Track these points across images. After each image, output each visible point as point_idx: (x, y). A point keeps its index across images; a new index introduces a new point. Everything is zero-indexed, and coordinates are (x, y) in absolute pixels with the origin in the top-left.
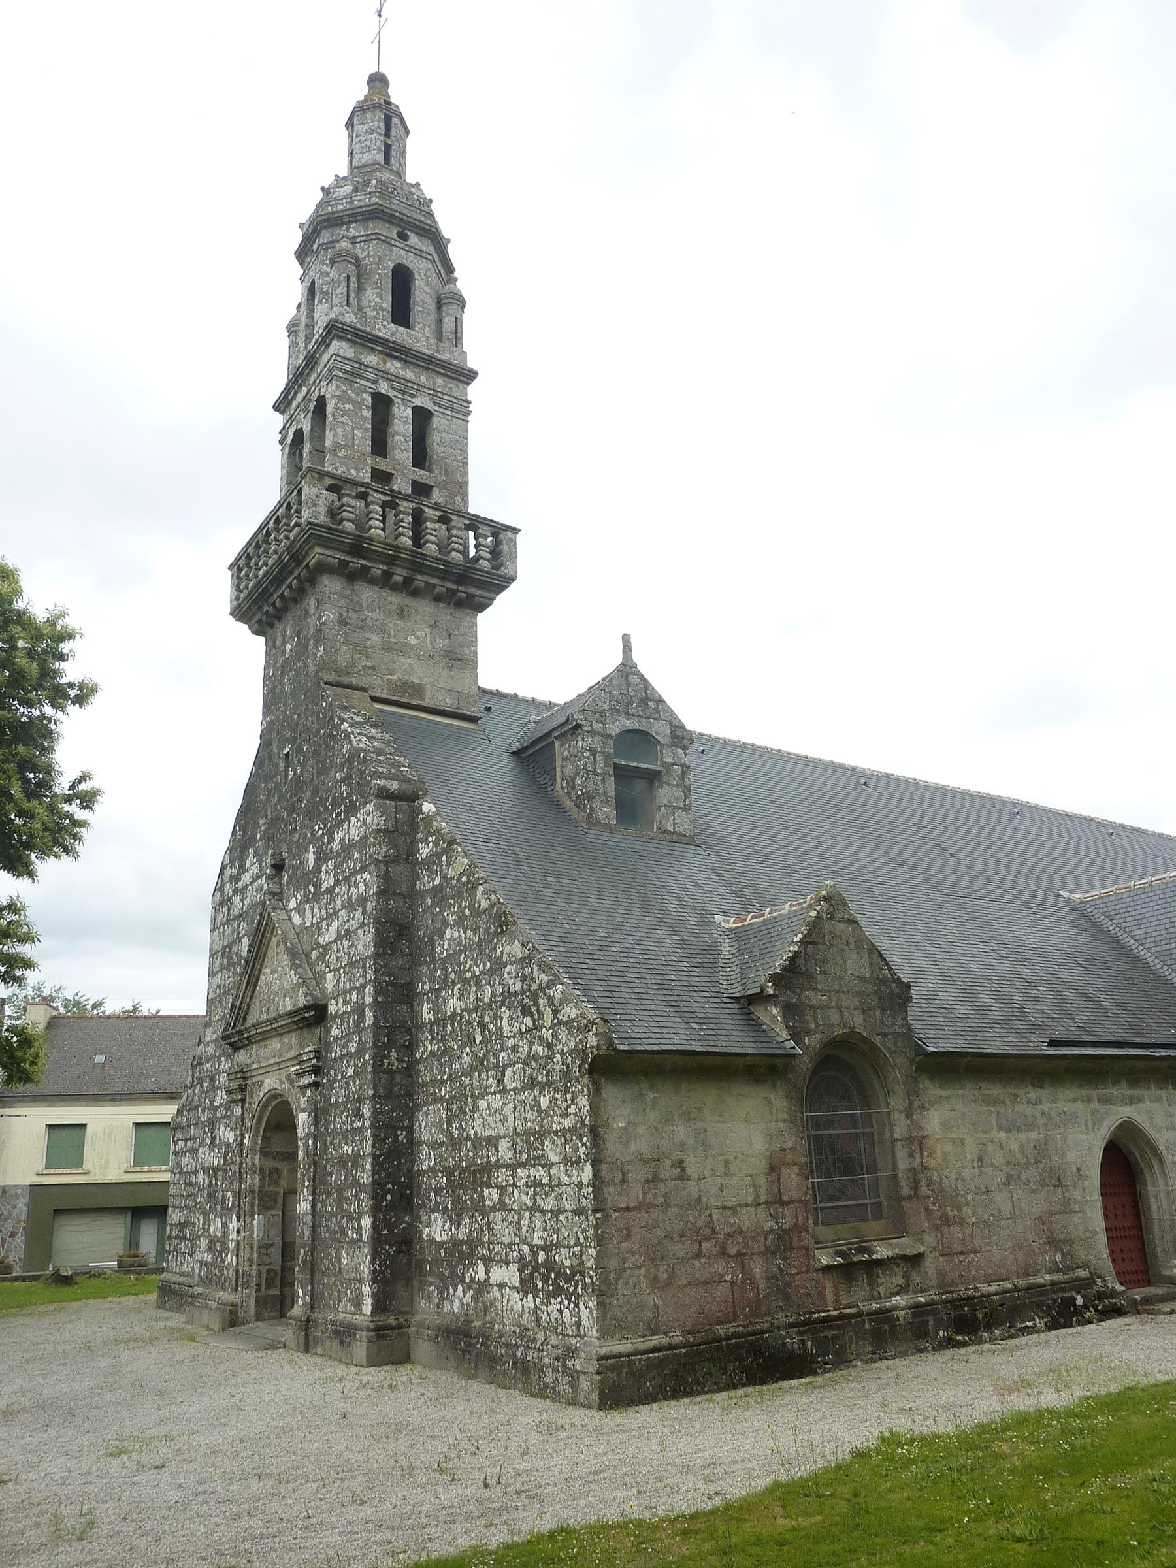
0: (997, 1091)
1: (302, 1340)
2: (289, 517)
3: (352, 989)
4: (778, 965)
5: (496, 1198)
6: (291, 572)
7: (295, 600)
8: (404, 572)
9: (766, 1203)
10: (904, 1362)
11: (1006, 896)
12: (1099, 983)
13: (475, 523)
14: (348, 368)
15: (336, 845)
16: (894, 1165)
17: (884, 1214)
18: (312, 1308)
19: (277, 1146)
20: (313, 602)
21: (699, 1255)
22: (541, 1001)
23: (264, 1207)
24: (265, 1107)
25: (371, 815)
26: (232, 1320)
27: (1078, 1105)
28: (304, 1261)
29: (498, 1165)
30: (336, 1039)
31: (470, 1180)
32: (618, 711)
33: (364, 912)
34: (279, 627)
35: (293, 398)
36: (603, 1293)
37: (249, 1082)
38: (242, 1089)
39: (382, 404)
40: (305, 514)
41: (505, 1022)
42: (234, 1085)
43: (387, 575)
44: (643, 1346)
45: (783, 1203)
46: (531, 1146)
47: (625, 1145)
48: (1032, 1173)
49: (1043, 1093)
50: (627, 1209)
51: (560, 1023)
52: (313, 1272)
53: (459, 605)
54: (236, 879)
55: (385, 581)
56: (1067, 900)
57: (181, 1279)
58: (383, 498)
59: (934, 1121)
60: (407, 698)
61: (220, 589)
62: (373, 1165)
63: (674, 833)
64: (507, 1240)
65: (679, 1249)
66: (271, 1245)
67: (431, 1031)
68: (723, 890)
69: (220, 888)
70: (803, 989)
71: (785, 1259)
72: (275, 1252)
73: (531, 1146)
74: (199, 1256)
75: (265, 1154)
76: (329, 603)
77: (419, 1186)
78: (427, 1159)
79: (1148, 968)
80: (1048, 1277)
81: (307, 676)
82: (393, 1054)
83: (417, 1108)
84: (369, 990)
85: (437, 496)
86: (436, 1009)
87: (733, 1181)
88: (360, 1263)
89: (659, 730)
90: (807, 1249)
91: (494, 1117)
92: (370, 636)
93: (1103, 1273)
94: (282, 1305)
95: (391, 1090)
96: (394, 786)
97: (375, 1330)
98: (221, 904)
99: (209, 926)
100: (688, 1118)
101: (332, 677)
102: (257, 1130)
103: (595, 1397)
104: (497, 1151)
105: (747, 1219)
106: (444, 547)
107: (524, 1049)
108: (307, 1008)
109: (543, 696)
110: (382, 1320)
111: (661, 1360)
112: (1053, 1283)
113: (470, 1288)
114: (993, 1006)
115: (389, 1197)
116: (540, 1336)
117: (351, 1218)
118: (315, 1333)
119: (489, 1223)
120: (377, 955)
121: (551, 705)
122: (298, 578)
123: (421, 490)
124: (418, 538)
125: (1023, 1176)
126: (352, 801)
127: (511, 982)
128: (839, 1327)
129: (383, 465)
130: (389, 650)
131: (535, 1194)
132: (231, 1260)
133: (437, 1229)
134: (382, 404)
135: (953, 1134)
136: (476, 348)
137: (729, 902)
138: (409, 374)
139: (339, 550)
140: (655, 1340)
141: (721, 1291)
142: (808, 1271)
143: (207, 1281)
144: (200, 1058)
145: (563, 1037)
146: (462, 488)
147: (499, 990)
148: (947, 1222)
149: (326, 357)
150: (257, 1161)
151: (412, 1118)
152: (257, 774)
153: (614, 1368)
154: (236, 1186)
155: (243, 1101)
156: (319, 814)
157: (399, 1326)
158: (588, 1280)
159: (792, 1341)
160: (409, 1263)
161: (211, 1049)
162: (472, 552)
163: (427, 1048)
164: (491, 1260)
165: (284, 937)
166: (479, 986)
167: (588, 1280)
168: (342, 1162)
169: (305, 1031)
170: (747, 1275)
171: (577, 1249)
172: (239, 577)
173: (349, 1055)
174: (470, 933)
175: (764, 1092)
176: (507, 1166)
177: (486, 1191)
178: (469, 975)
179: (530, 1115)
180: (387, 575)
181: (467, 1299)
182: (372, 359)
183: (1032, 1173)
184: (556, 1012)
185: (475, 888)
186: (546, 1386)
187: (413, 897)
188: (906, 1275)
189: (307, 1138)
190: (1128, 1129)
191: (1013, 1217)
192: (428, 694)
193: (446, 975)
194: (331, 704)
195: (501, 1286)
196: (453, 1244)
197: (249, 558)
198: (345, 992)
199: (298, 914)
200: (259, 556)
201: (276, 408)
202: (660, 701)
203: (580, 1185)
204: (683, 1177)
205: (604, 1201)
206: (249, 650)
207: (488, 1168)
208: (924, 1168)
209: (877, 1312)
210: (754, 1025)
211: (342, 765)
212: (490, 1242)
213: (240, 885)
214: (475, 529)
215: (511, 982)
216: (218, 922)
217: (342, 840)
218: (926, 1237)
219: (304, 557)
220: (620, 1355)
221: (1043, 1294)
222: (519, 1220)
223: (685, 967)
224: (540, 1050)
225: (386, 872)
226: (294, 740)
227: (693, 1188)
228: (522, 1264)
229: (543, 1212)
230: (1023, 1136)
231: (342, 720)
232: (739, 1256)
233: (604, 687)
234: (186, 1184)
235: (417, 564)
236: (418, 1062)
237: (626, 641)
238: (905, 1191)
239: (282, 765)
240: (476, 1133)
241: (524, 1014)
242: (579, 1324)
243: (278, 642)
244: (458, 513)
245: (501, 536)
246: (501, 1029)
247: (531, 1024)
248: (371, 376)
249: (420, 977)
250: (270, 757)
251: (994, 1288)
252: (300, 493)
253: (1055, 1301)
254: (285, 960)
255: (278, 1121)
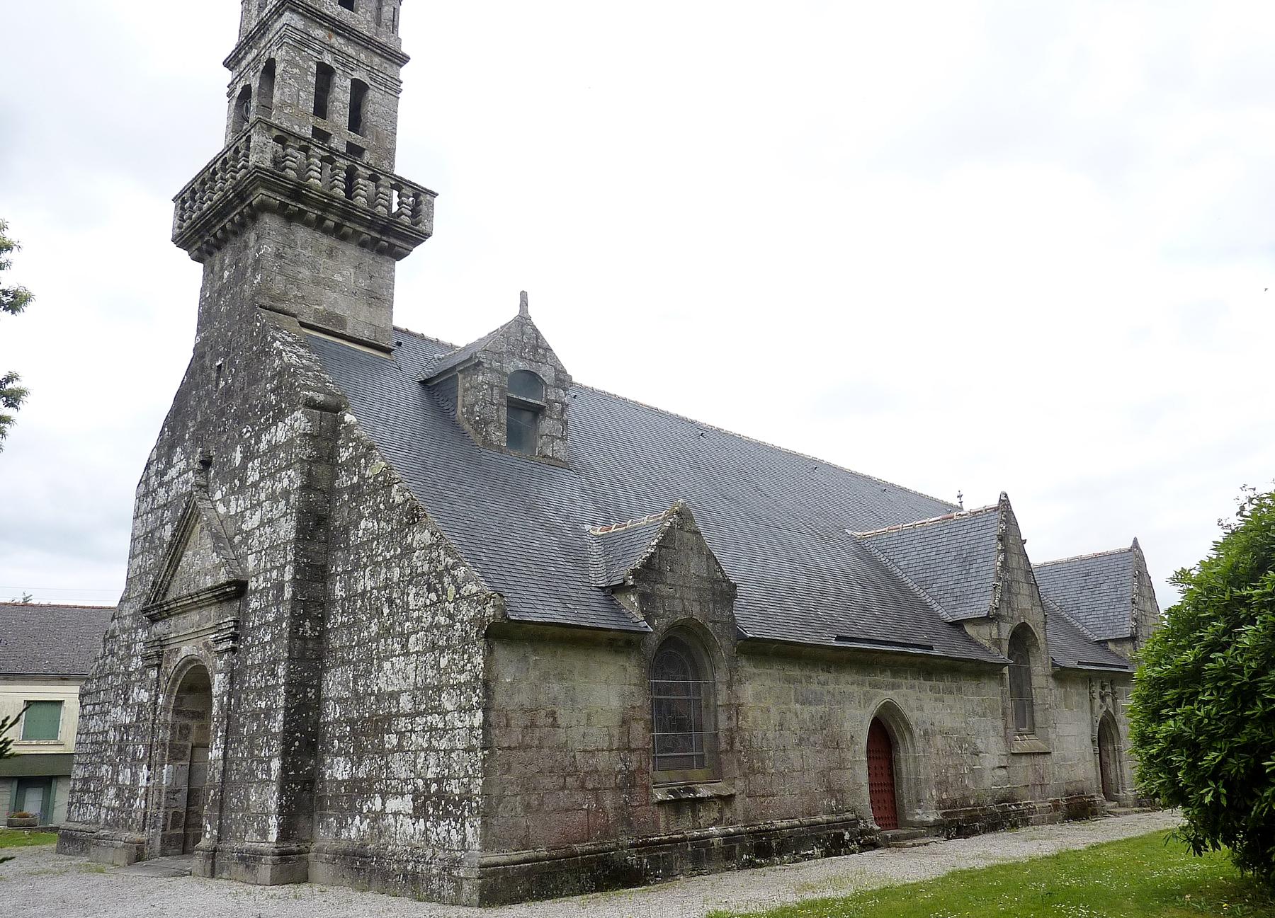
0: (796, 672)
1: (208, 867)
2: (237, 160)
3: (273, 568)
4: (637, 563)
5: (395, 742)
6: (235, 208)
7: (235, 234)
8: (335, 219)
9: (618, 749)
10: (717, 876)
11: (805, 530)
12: (873, 598)
13: (400, 184)
14: (298, 38)
15: (263, 446)
16: (716, 724)
17: (706, 764)
18: (219, 840)
19: (190, 704)
20: (253, 236)
21: (563, 788)
22: (445, 580)
23: (174, 759)
24: (181, 670)
25: (299, 421)
26: (138, 856)
27: (855, 687)
28: (214, 801)
29: (398, 715)
30: (255, 611)
31: (371, 730)
32: (513, 354)
33: (287, 503)
34: (218, 255)
35: (243, 58)
36: (486, 815)
37: (166, 650)
38: (159, 655)
39: (325, 73)
40: (253, 159)
41: (411, 598)
42: (152, 652)
43: (321, 220)
44: (516, 858)
45: (631, 750)
46: (430, 698)
47: (510, 697)
48: (817, 738)
49: (830, 677)
50: (509, 748)
51: (462, 597)
52: (221, 810)
53: (381, 252)
54: (163, 473)
55: (318, 225)
56: (850, 536)
57: (82, 827)
58: (322, 153)
59: (748, 692)
60: (331, 327)
61: (165, 218)
62: (285, 716)
63: (552, 458)
64: (403, 776)
65: (548, 782)
66: (178, 791)
67: (343, 606)
68: (590, 505)
69: (145, 481)
70: (655, 582)
71: (630, 794)
72: (182, 797)
73: (430, 698)
74: (106, 803)
75: (177, 712)
76: (268, 238)
77: (324, 735)
78: (333, 712)
79: (909, 591)
80: (825, 817)
81: (242, 300)
82: (308, 624)
83: (326, 669)
84: (289, 570)
85: (368, 157)
86: (347, 587)
87: (594, 730)
88: (267, 799)
89: (546, 373)
90: (647, 788)
91: (397, 675)
92: (301, 270)
93: (865, 816)
94: (185, 843)
95: (303, 654)
96: (320, 398)
97: (279, 855)
98: (146, 495)
99: (132, 514)
100: (561, 677)
101: (267, 302)
102: (172, 691)
103: (476, 897)
104: (398, 703)
105: (602, 761)
106: (373, 202)
107: (427, 619)
108: (229, 584)
109: (445, 338)
110: (286, 846)
111: (530, 869)
112: (828, 822)
113: (367, 817)
114: (795, 608)
115: (297, 743)
116: (429, 852)
117: (261, 761)
118: (221, 860)
119: (387, 763)
120: (297, 540)
121: (452, 347)
122: (240, 214)
123: (354, 151)
124: (349, 191)
125: (812, 739)
126: (280, 410)
127: (419, 564)
128: (668, 849)
129: (323, 126)
130: (318, 284)
131: (431, 737)
132: (139, 804)
133: (339, 770)
134: (325, 73)
135: (762, 705)
136: (409, 37)
137: (595, 515)
138: (351, 51)
139: (281, 194)
140: (526, 854)
141: (580, 817)
142: (647, 804)
143: (114, 824)
144: (114, 631)
145: (464, 609)
146: (390, 153)
147: (408, 571)
148: (754, 771)
149: (277, 26)
150: (169, 719)
151: (320, 678)
152: (188, 382)
153: (493, 874)
154: (148, 740)
155: (159, 666)
156: (248, 418)
157: (300, 852)
158: (474, 805)
159: (632, 859)
160: (311, 799)
161: (128, 622)
162: (395, 208)
163: (338, 619)
164: (387, 793)
165: (209, 524)
166: (389, 568)
167: (474, 805)
168: (255, 715)
169: (225, 604)
170: (600, 806)
171: (466, 780)
172: (182, 209)
173: (267, 624)
174: (383, 524)
175: (622, 661)
176: (405, 716)
177: (386, 737)
178: (380, 559)
179: (430, 673)
180: (321, 220)
181: (364, 826)
182: (319, 33)
183: (817, 738)
184: (458, 589)
185: (390, 486)
186: (432, 892)
187: (331, 493)
188: (720, 811)
189: (222, 695)
190: (889, 707)
191: (802, 770)
192: (349, 325)
193: (358, 559)
194: (264, 325)
195: (396, 814)
196: (354, 782)
197: (194, 192)
198: (266, 571)
199: (222, 503)
200: (204, 192)
201: (227, 64)
202: (548, 349)
203: (472, 728)
204: (554, 725)
205: (491, 742)
206: (188, 274)
207: (389, 717)
208: (739, 729)
209: (697, 838)
210: (617, 609)
211: (273, 378)
212: (387, 779)
213: (166, 478)
214: (398, 188)
215: (419, 564)
216: (142, 510)
217: (269, 442)
218: (737, 782)
219: (248, 196)
220: (497, 865)
221: (821, 829)
222: (415, 758)
223: (561, 561)
224: (442, 620)
225: (310, 470)
226: (228, 354)
227: (561, 735)
228: (416, 794)
229: (437, 751)
230: (813, 708)
231: (275, 339)
232: (594, 789)
233: (504, 333)
234: (92, 743)
235: (348, 213)
236: (329, 631)
237: (524, 296)
238: (723, 746)
239: (214, 375)
240: (380, 689)
241: (429, 591)
242: (464, 840)
243: (217, 268)
244: (387, 174)
245: (420, 197)
246: (408, 603)
247: (435, 599)
248: (317, 47)
249: (334, 561)
250: (203, 368)
251: (785, 823)
252: (248, 140)
253: (829, 835)
254: (209, 543)
255: (194, 684)
